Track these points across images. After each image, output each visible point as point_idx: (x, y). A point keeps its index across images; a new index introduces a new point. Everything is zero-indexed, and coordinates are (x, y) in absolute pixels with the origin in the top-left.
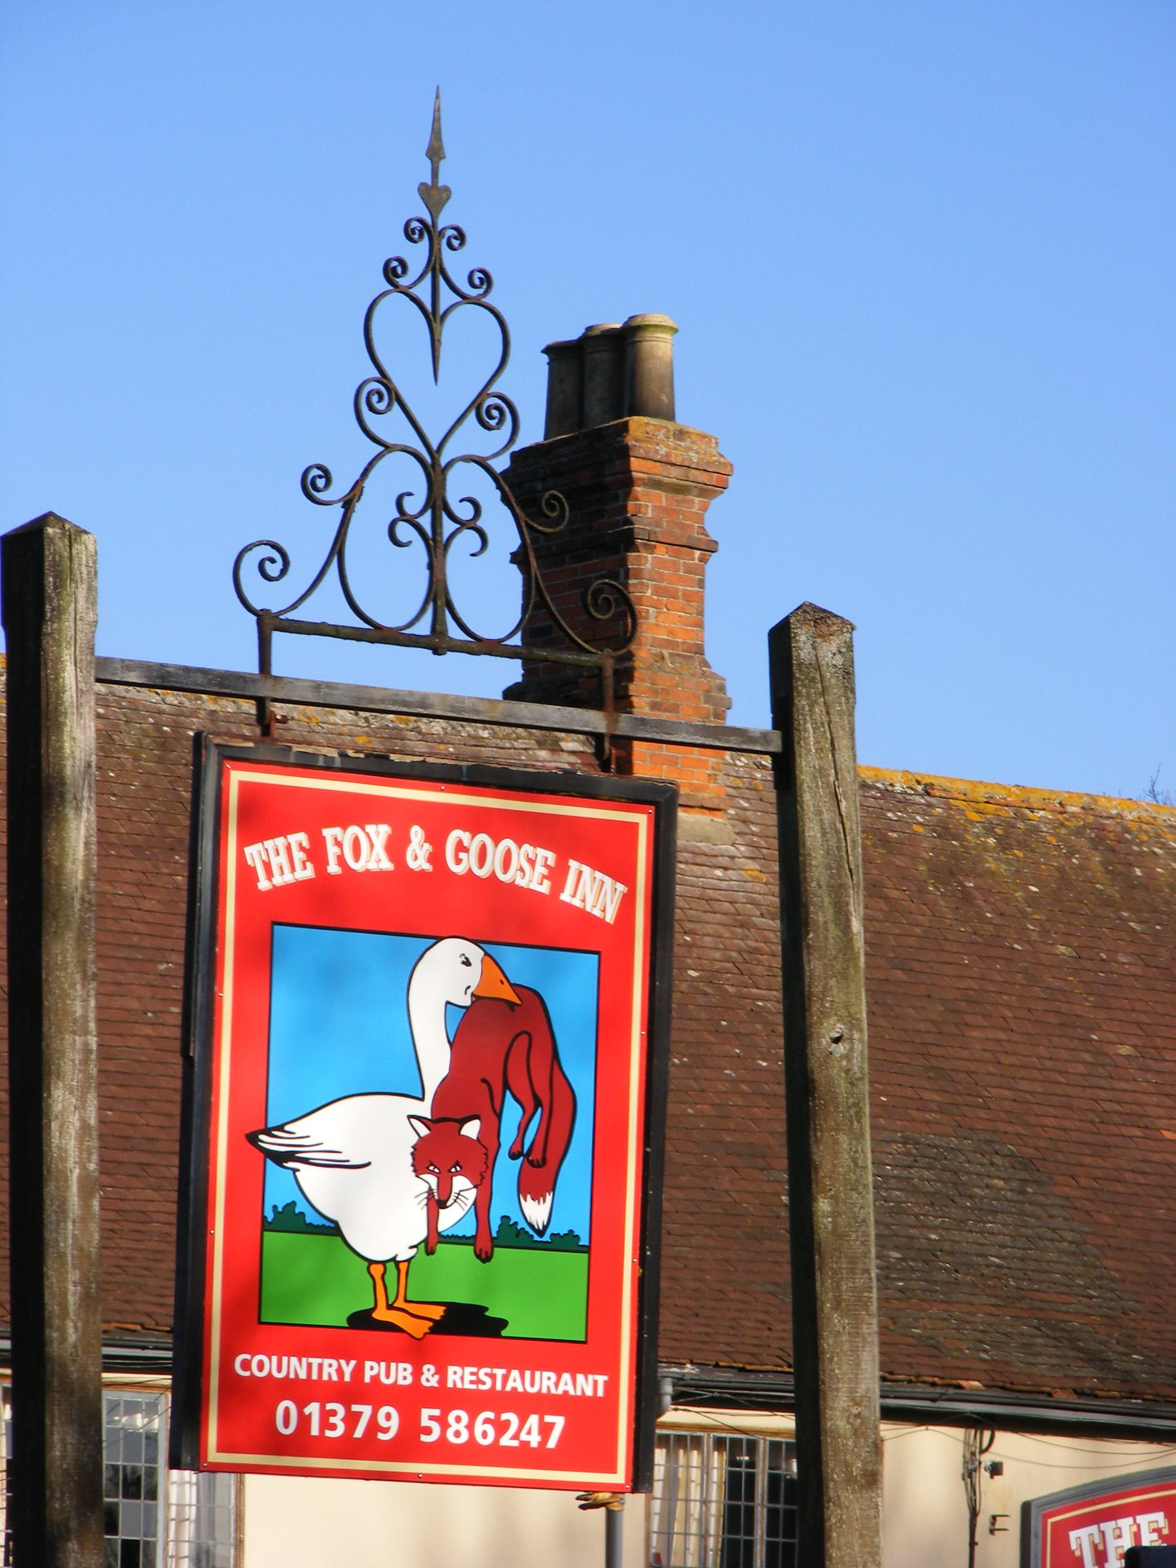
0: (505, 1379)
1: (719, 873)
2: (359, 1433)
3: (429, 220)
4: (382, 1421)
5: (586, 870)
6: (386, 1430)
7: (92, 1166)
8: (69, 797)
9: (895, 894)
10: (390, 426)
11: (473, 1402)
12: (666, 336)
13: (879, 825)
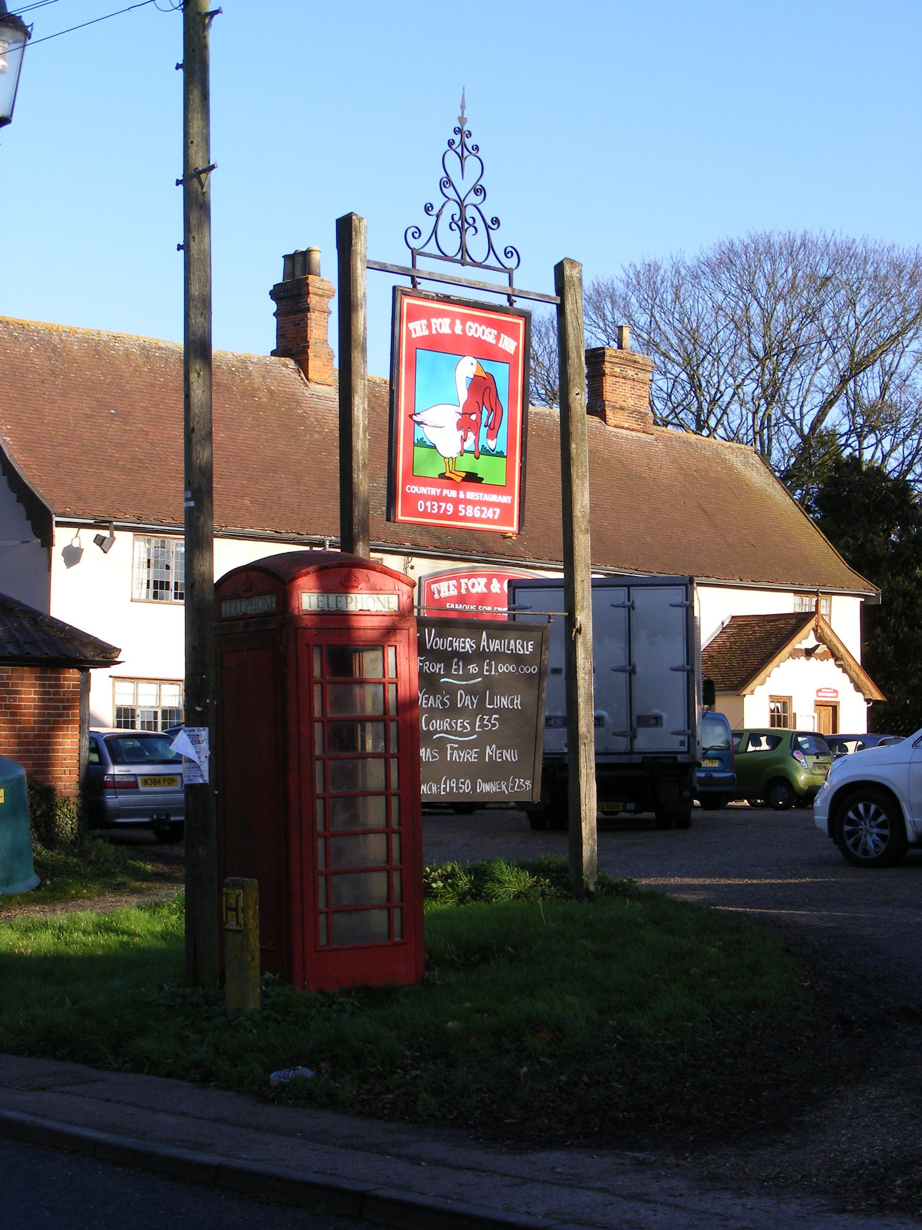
0: (483, 496)
1: (332, 403)
2: (441, 512)
3: (461, 127)
4: (448, 508)
5: (506, 337)
6: (449, 511)
7: (366, 422)
8: (359, 303)
9: (379, 411)
10: (449, 192)
11: (474, 503)
12: (318, 253)
13: (373, 391)
